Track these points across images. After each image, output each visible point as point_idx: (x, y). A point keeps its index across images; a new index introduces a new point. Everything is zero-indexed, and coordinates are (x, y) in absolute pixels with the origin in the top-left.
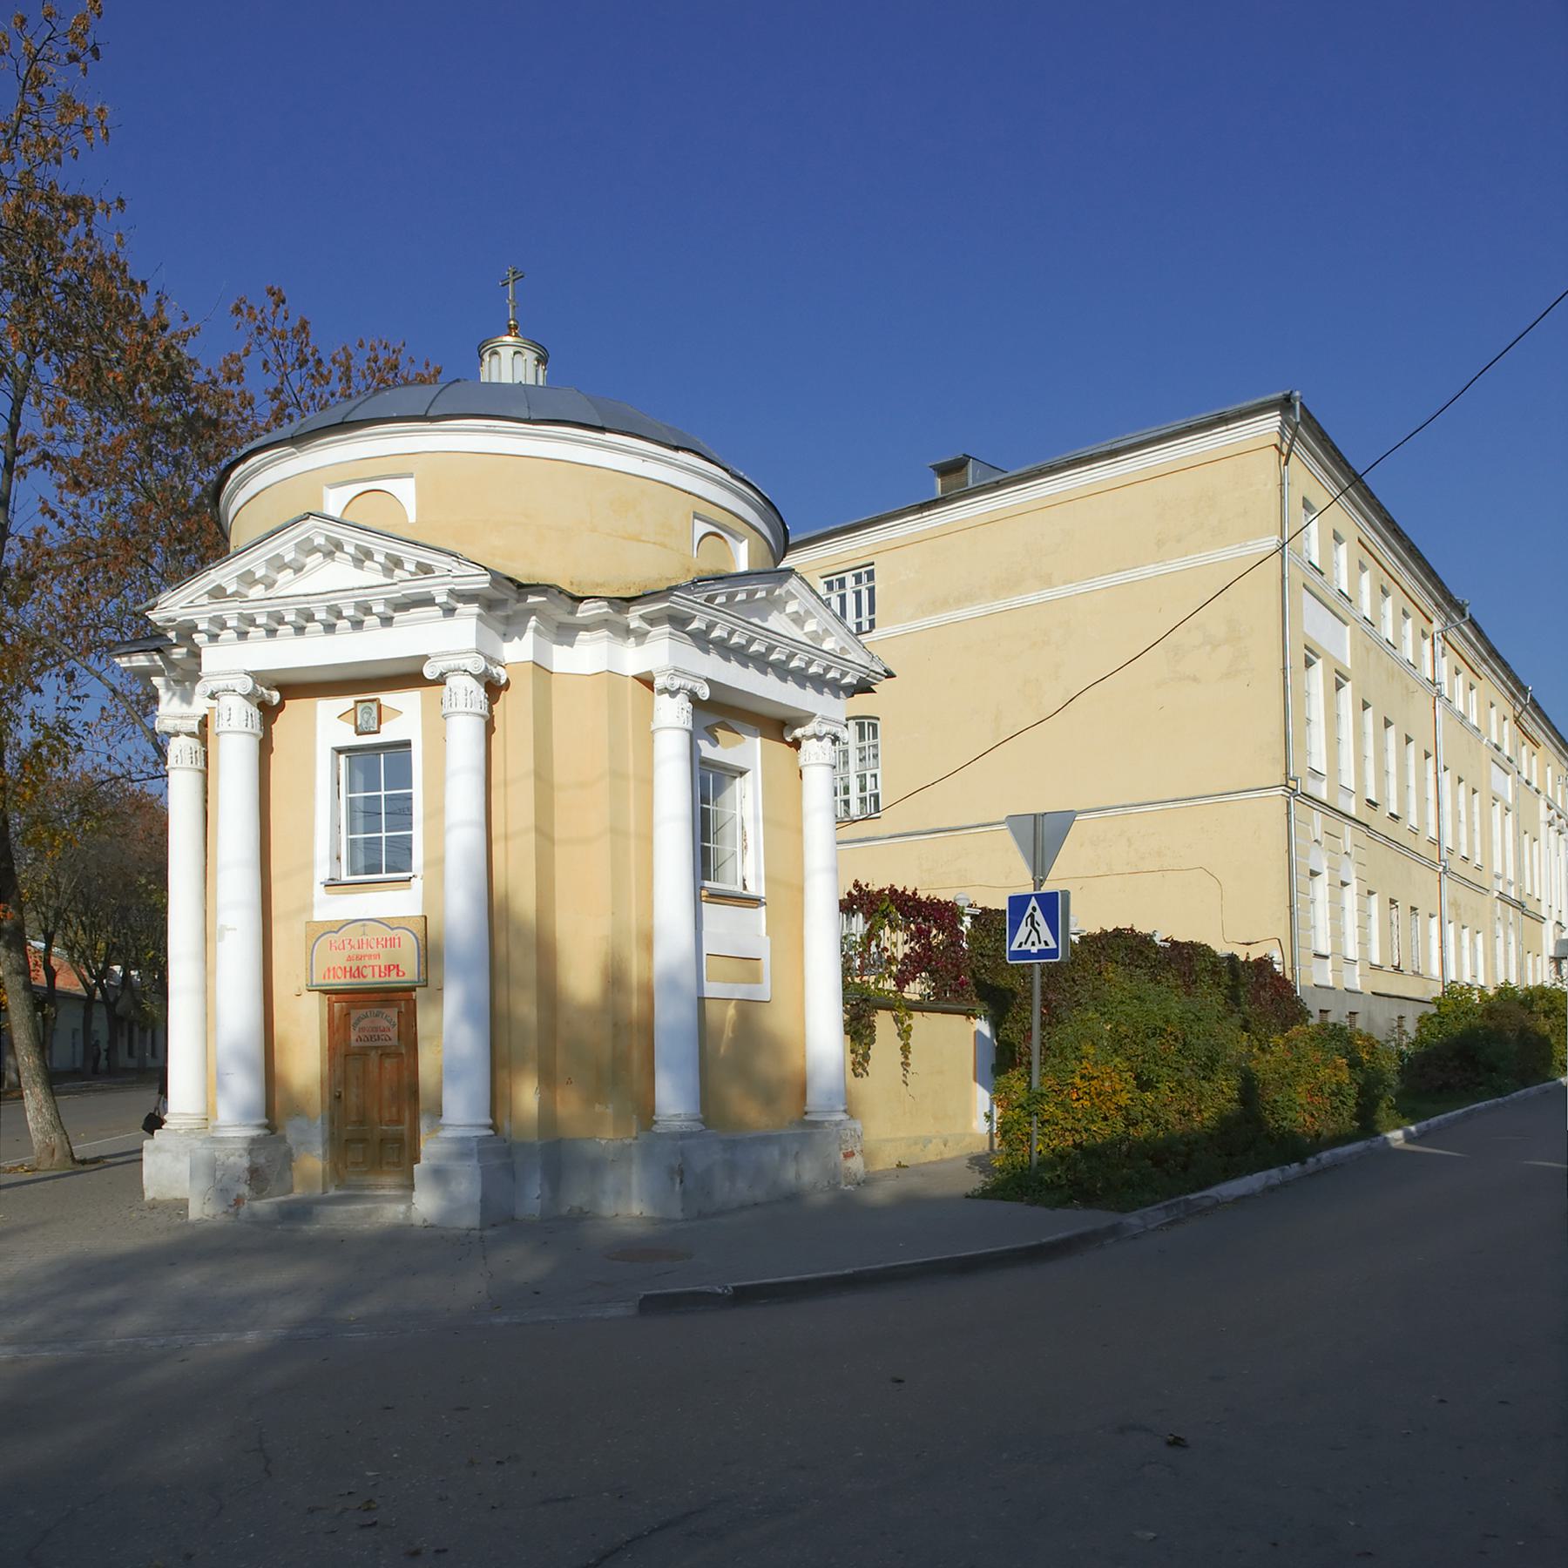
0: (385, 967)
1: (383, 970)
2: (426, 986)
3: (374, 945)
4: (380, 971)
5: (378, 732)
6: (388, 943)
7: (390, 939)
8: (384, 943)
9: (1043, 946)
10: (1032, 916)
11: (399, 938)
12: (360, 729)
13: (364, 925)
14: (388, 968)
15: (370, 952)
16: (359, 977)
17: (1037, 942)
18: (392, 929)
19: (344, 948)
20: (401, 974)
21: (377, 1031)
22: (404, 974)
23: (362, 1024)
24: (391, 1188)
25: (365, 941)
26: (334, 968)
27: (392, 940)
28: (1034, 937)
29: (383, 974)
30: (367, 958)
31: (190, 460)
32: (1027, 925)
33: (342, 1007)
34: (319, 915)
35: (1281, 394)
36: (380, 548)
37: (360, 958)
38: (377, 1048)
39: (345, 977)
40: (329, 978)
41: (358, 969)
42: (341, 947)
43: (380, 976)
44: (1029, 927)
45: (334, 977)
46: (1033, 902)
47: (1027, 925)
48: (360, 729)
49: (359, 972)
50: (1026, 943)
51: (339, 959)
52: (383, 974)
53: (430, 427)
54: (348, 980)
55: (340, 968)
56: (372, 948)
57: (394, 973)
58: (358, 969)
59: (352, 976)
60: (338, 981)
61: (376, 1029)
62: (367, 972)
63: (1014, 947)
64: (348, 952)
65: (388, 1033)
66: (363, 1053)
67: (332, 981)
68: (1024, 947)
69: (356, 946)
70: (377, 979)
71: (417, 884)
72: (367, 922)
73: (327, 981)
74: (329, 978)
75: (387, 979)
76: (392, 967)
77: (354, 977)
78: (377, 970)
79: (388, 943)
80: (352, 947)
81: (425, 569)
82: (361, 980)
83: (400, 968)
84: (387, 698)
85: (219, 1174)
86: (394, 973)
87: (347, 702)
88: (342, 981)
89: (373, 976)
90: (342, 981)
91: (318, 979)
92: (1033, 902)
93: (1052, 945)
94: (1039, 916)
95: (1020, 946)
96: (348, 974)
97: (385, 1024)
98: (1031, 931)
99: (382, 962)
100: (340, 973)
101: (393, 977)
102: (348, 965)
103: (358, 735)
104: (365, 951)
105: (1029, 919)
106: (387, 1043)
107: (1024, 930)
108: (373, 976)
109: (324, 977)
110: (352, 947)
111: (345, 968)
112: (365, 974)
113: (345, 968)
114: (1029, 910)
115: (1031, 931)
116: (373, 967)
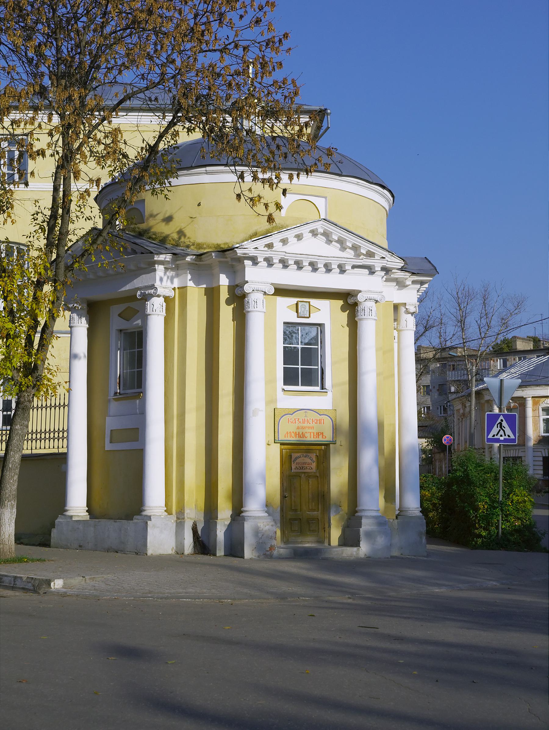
0: (316, 433)
1: (315, 434)
2: (275, 442)
3: (311, 421)
4: (314, 436)
5: (308, 318)
6: (318, 421)
7: (319, 420)
8: (316, 421)
9: (507, 437)
10: (501, 424)
11: (323, 420)
12: (300, 315)
13: (306, 412)
14: (318, 434)
15: (308, 425)
16: (303, 437)
17: (503, 435)
18: (320, 415)
19: (295, 423)
20: (324, 437)
21: (305, 464)
22: (326, 437)
23: (298, 461)
24: (312, 542)
25: (306, 420)
26: (290, 432)
27: (320, 420)
28: (502, 432)
29: (315, 437)
30: (307, 428)
31: (248, 178)
32: (497, 427)
33: (287, 452)
34: (280, 405)
35: (318, 108)
36: (350, 241)
37: (303, 428)
38: (305, 473)
39: (296, 437)
40: (287, 437)
41: (303, 433)
42: (294, 422)
43: (314, 438)
44: (499, 428)
45: (290, 437)
46: (501, 417)
47: (497, 427)
48: (300, 315)
49: (303, 435)
50: (497, 435)
51: (292, 428)
52: (315, 437)
53: (338, 178)
54: (297, 439)
55: (293, 432)
56: (309, 423)
57: (320, 437)
58: (303, 433)
59: (300, 437)
60: (291, 439)
61: (305, 463)
62: (307, 435)
63: (490, 436)
64: (297, 425)
65: (311, 466)
66: (297, 476)
67: (289, 439)
68: (496, 437)
69: (302, 422)
70: (312, 439)
71: (330, 394)
72: (308, 411)
73: (286, 439)
74: (287, 437)
75: (317, 439)
76: (320, 434)
77: (301, 437)
78: (312, 435)
79: (318, 421)
80: (300, 422)
81: (370, 255)
82: (305, 439)
83: (324, 434)
84: (314, 302)
85: (260, 535)
86: (320, 437)
87: (294, 300)
88: (293, 439)
89: (311, 437)
90: (294, 439)
91: (282, 437)
92: (501, 417)
93: (512, 437)
94: (504, 424)
95: (494, 436)
96: (297, 436)
97: (309, 461)
98: (500, 430)
99: (315, 431)
100: (293, 435)
101: (320, 438)
102: (297, 431)
103: (298, 317)
104: (306, 425)
105: (499, 425)
106: (309, 471)
107: (495, 430)
108: (311, 437)
109: (285, 437)
110: (300, 422)
111: (296, 432)
112: (306, 436)
113: (296, 432)
114: (499, 421)
115: (500, 430)
116: (310, 433)
